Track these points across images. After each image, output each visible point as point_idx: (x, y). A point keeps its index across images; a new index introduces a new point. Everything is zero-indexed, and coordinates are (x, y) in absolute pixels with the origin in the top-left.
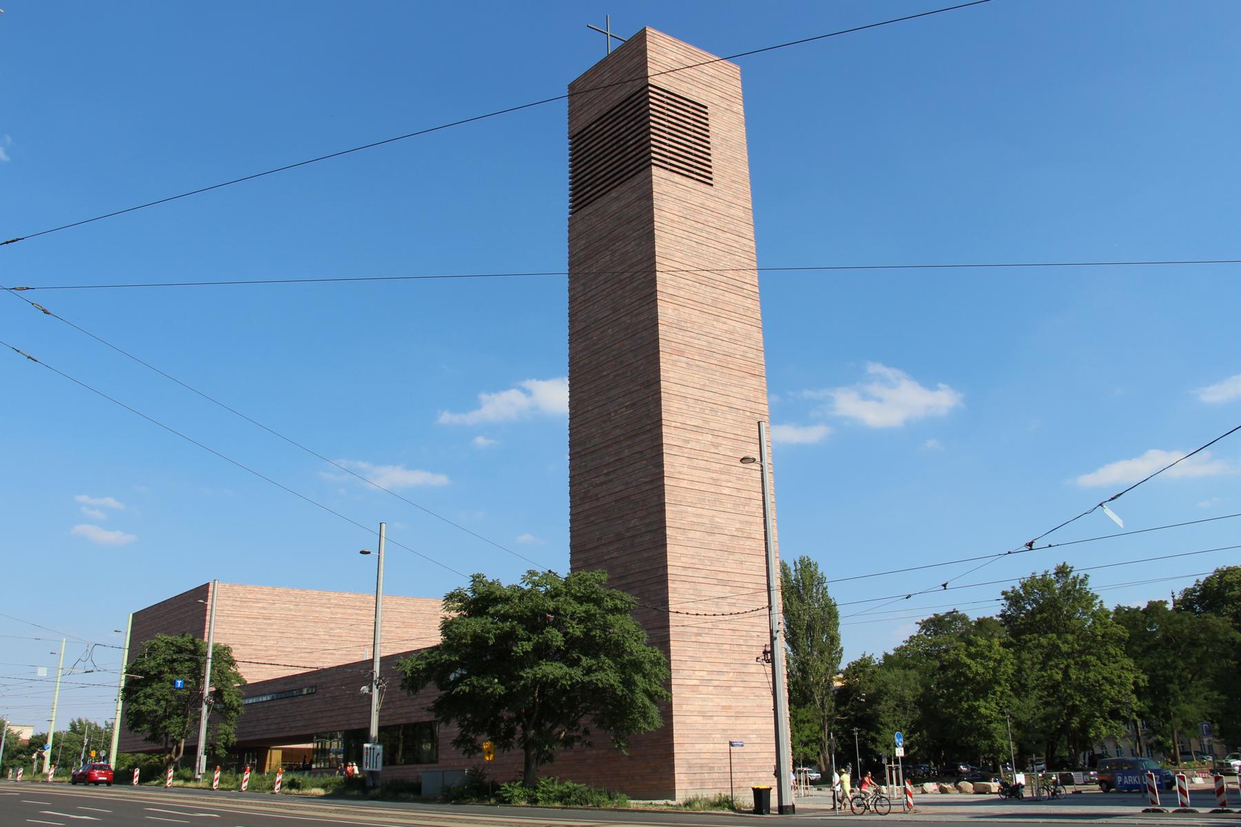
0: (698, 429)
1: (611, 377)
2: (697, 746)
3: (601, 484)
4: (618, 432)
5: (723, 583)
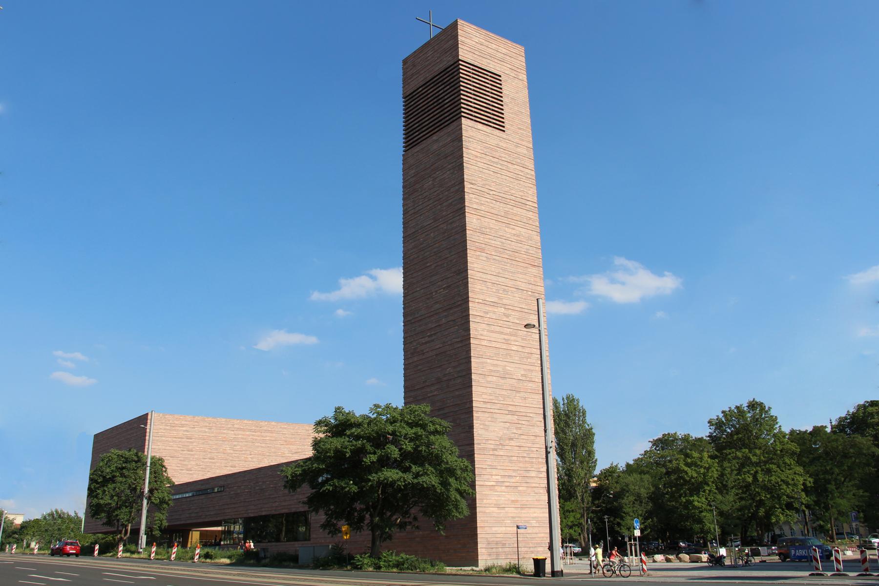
0: (494, 304)
1: (433, 267)
2: (494, 529)
4: (437, 306)
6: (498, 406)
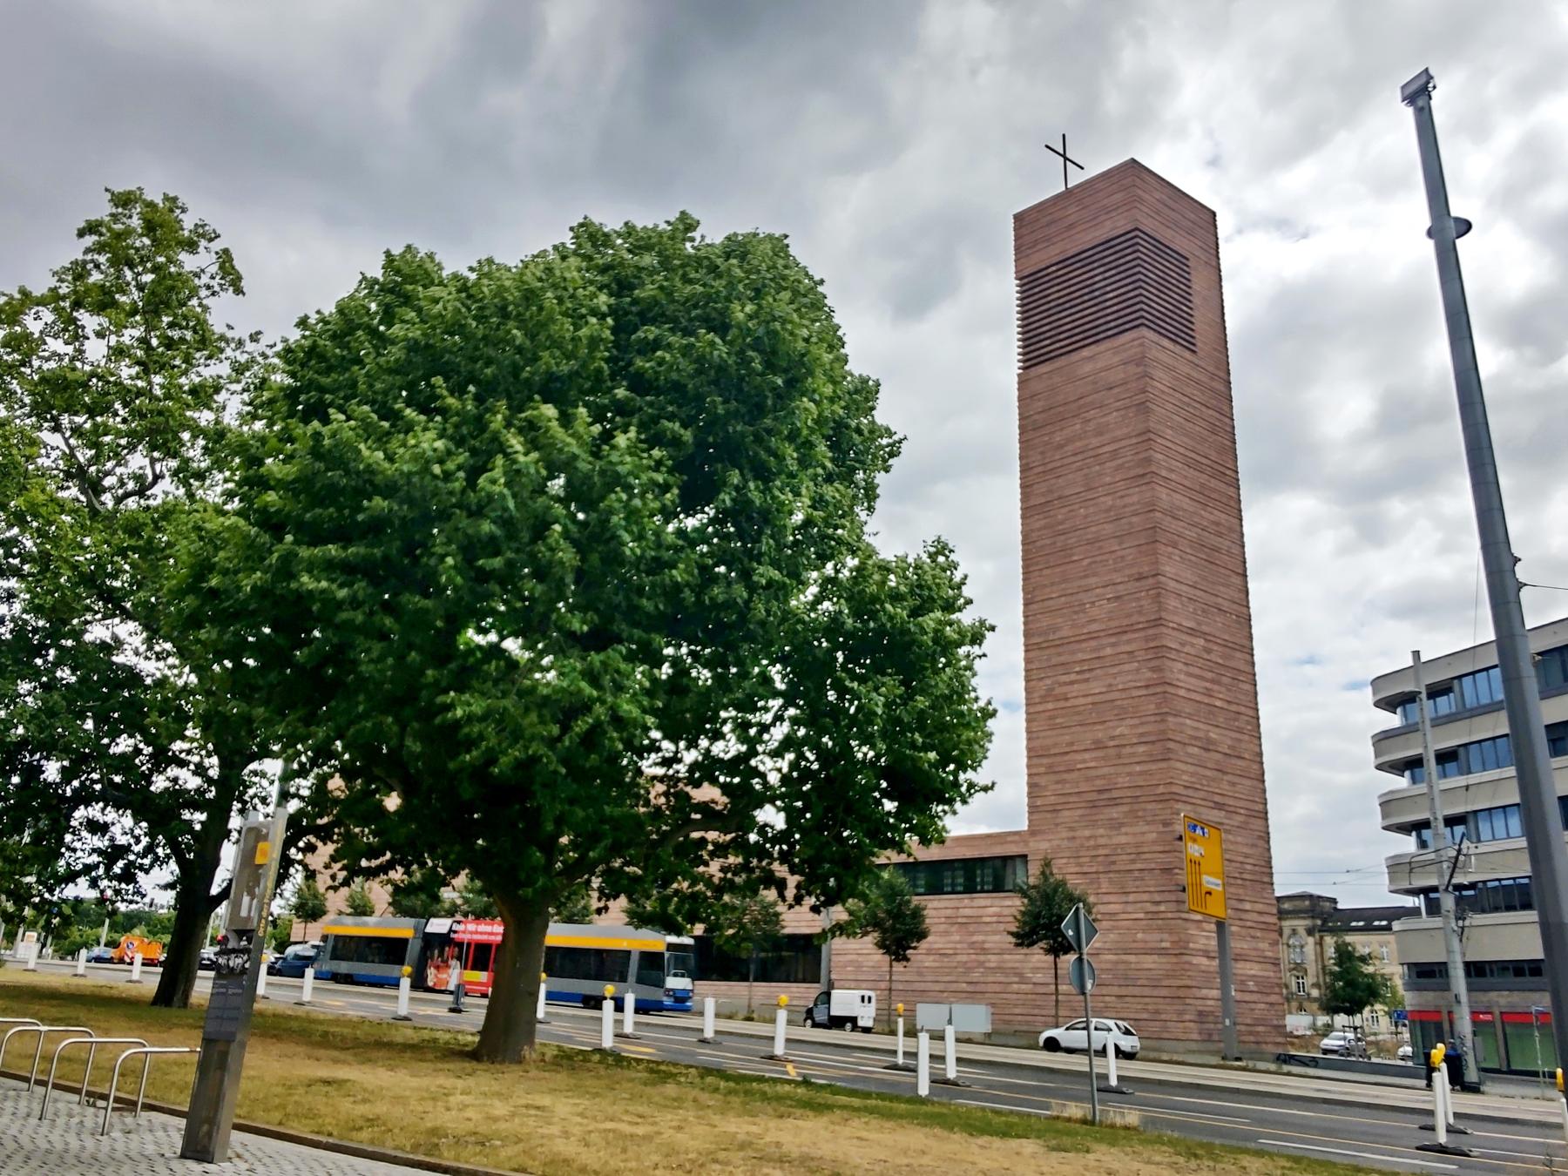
0: (1192, 632)
1: (1085, 562)
2: (1204, 992)
3: (1072, 683)
5: (1219, 806)
6: (1201, 795)
